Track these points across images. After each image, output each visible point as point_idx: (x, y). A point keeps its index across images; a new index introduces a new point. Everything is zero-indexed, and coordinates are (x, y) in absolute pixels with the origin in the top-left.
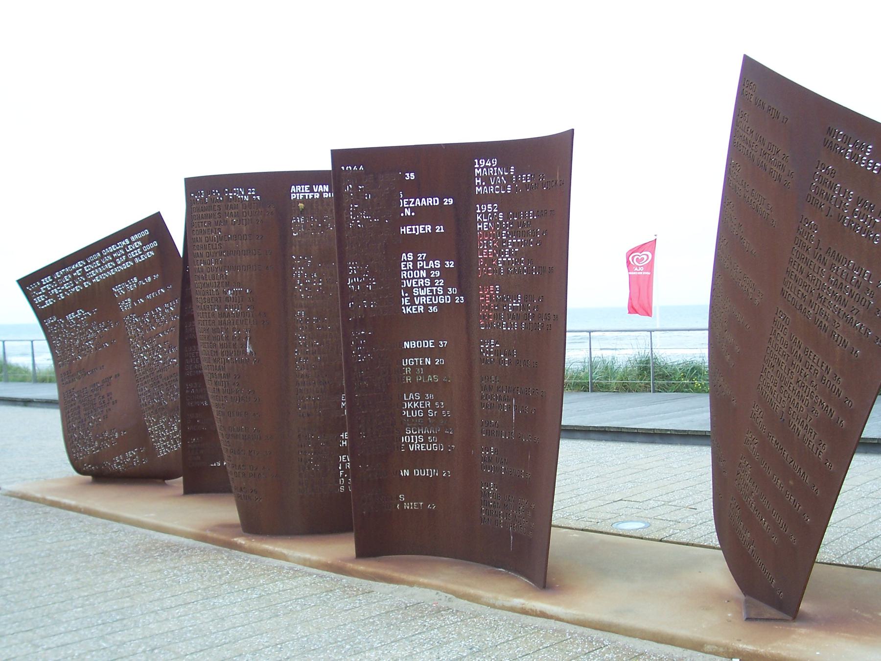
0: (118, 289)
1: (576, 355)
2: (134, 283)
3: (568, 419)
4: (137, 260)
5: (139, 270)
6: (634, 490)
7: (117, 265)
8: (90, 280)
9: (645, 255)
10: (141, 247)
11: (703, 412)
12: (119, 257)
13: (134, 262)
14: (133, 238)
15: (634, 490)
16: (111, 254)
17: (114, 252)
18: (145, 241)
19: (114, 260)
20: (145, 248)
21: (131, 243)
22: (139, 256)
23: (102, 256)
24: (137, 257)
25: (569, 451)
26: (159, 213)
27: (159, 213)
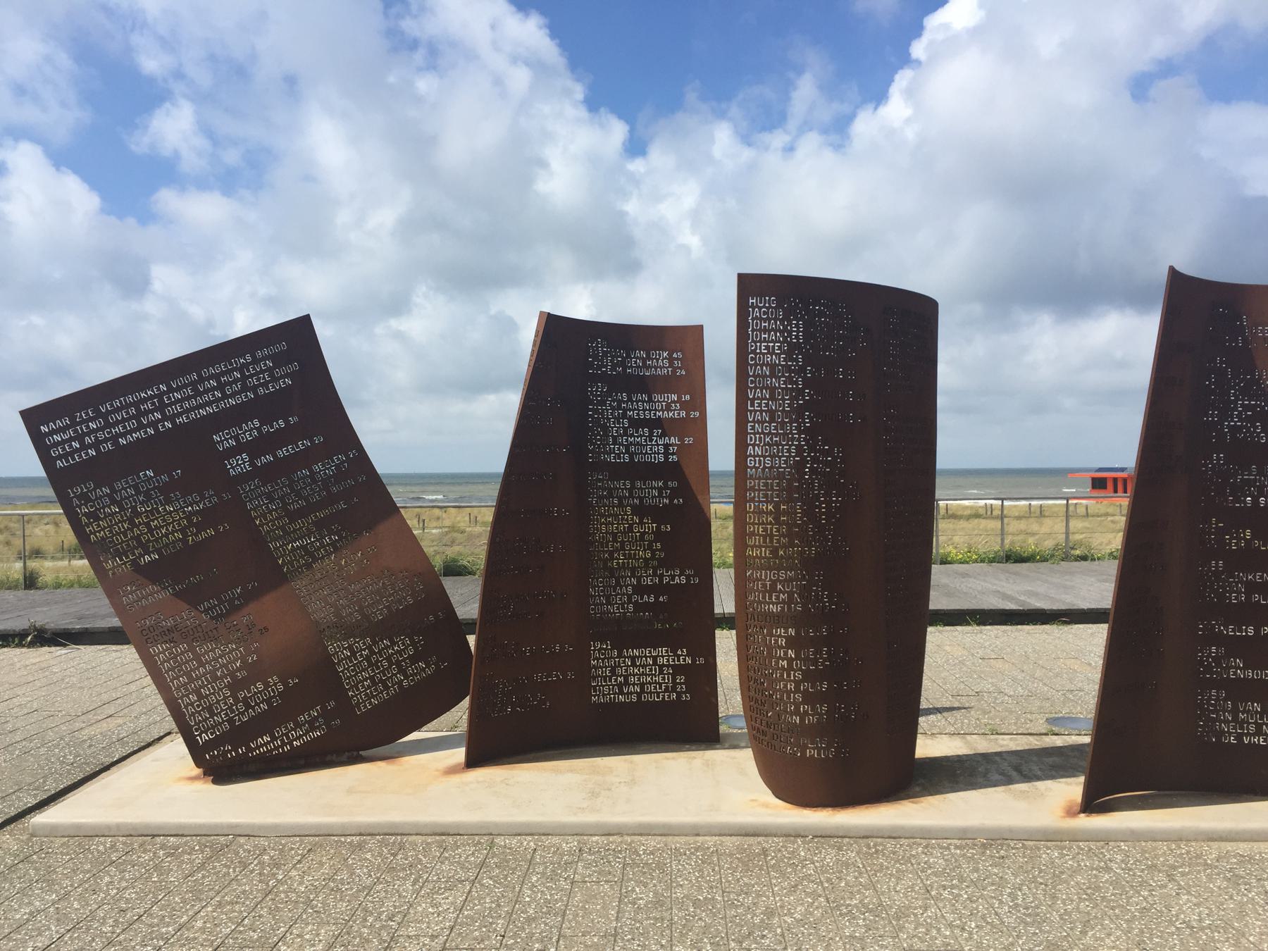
0: (224, 440)
1: (1124, 502)
2: (250, 430)
3: (937, 602)
4: (261, 391)
5: (263, 408)
6: (1012, 672)
7: (225, 397)
8: (172, 418)
9: (1043, 404)
10: (270, 370)
11: (1105, 581)
12: (230, 384)
13: (256, 393)
14: (259, 354)
15: (1012, 672)
16: (216, 377)
17: (223, 374)
18: (279, 360)
19: (221, 387)
20: (278, 372)
21: (255, 361)
22: (265, 385)
23: (202, 380)
24: (261, 385)
25: (936, 637)
26: (740, 276)
27: (740, 276)
